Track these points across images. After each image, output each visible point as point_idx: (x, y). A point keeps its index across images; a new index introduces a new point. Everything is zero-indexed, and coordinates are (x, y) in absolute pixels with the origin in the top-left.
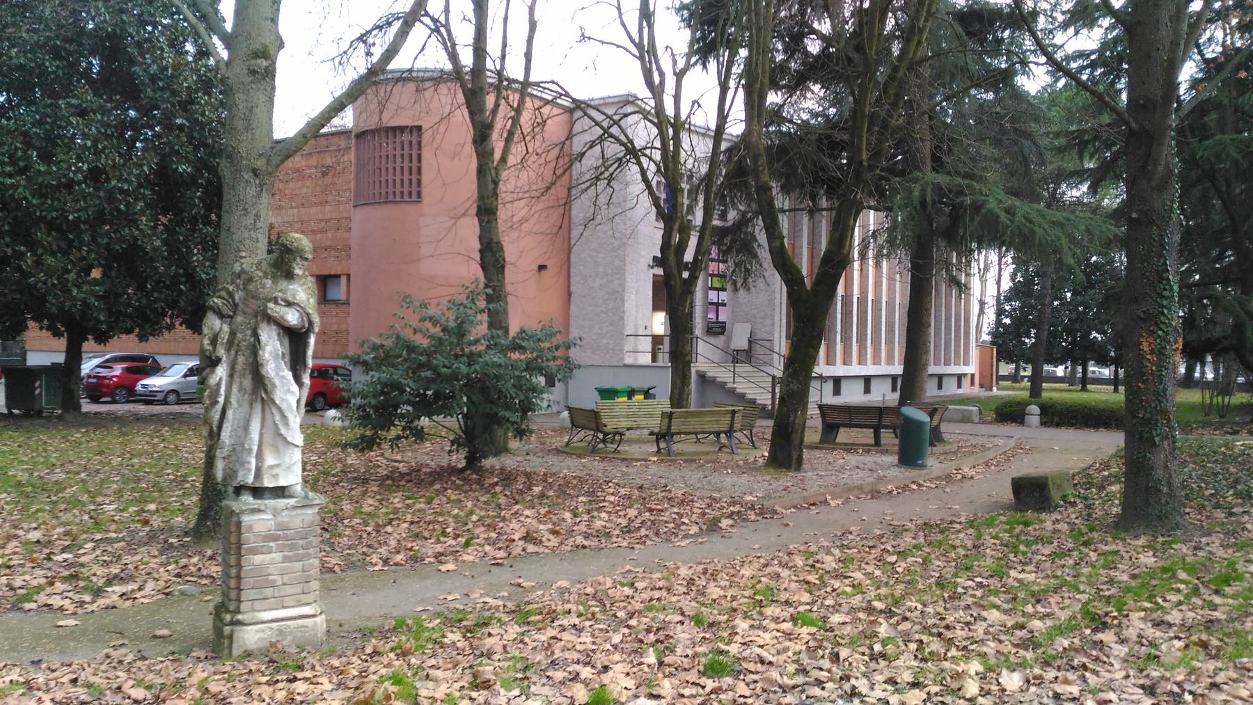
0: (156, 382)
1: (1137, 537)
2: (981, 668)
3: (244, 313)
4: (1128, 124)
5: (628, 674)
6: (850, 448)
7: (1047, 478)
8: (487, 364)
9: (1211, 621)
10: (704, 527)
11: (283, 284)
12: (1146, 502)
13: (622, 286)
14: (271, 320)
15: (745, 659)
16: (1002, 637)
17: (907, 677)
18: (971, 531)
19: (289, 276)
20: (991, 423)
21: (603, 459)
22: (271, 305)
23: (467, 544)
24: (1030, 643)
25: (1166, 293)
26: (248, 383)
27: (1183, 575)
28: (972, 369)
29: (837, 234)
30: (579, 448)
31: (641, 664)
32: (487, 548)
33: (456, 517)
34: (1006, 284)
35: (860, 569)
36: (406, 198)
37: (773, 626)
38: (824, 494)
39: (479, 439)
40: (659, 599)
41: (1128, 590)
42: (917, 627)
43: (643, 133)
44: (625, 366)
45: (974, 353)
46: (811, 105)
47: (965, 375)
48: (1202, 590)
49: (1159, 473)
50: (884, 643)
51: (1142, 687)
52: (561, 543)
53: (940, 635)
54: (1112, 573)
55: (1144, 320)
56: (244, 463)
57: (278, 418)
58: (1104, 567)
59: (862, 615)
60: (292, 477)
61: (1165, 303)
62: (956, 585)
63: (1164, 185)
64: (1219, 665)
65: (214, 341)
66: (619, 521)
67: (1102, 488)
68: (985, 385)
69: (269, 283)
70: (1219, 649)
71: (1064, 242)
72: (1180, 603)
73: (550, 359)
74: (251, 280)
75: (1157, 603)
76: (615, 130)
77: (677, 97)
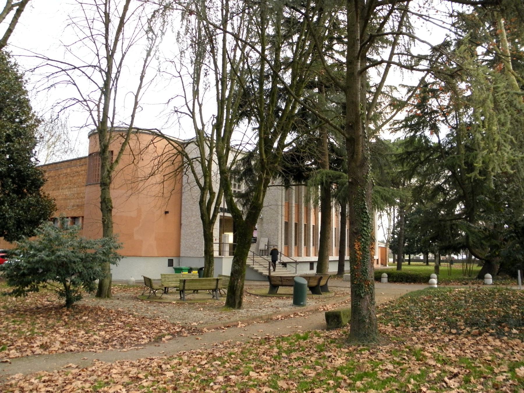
49: (365, 312)
61: (365, 224)
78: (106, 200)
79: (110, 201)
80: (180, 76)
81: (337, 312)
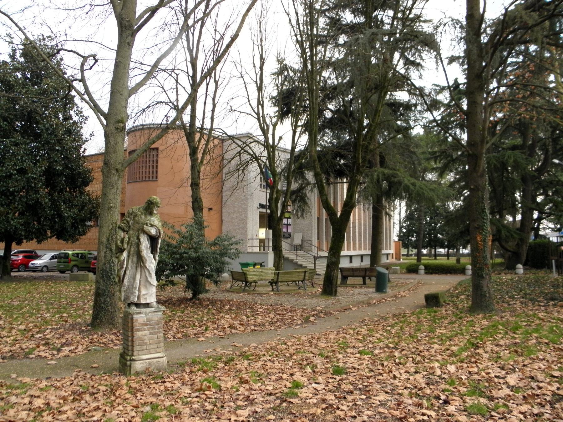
0: (38, 262)
1: (478, 314)
2: (439, 365)
3: (133, 230)
4: (468, 152)
5: (302, 376)
6: (353, 286)
7: (438, 294)
8: (204, 252)
9: (516, 343)
10: (303, 321)
11: (149, 217)
12: (480, 301)
13: (246, 217)
14: (144, 232)
15: (347, 368)
16: (443, 354)
17: (413, 370)
18: (415, 316)
19: (151, 214)
20: (405, 274)
21: (249, 294)
22: (145, 226)
23: (206, 330)
24: (453, 355)
25: (485, 217)
26: (135, 259)
27: (501, 327)
28: (392, 251)
29: (350, 194)
30: (236, 289)
31: (306, 372)
32: (215, 331)
33: (197, 318)
34: (403, 214)
35: (378, 333)
36: (151, 179)
37: (352, 356)
38: (349, 305)
39: (195, 285)
40: (300, 349)
41: (482, 334)
42: (409, 352)
43: (258, 150)
44: (248, 253)
45: (393, 245)
46: (327, 139)
47: (389, 254)
48: (509, 332)
49: (485, 289)
50: (400, 358)
51: (499, 367)
52: (245, 329)
53: (419, 354)
54: (474, 328)
55: (478, 228)
56: (133, 293)
57: (147, 274)
58: (470, 326)
59: (386, 349)
60: (152, 299)
62: (417, 336)
63: (482, 176)
64: (524, 358)
65: (122, 241)
66: (267, 319)
67: (458, 297)
68: (398, 258)
69: (143, 217)
70: (522, 353)
71: (435, 197)
72: (502, 338)
73: (224, 248)
74: (136, 216)
75: (494, 338)
76: (247, 148)
77: (273, 135)
78: (198, 199)
79: (202, 201)
80: (242, 77)
81: (436, 294)
